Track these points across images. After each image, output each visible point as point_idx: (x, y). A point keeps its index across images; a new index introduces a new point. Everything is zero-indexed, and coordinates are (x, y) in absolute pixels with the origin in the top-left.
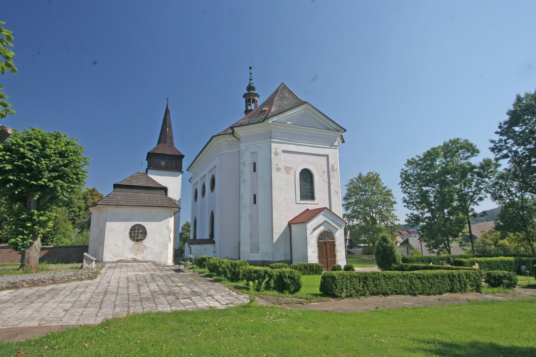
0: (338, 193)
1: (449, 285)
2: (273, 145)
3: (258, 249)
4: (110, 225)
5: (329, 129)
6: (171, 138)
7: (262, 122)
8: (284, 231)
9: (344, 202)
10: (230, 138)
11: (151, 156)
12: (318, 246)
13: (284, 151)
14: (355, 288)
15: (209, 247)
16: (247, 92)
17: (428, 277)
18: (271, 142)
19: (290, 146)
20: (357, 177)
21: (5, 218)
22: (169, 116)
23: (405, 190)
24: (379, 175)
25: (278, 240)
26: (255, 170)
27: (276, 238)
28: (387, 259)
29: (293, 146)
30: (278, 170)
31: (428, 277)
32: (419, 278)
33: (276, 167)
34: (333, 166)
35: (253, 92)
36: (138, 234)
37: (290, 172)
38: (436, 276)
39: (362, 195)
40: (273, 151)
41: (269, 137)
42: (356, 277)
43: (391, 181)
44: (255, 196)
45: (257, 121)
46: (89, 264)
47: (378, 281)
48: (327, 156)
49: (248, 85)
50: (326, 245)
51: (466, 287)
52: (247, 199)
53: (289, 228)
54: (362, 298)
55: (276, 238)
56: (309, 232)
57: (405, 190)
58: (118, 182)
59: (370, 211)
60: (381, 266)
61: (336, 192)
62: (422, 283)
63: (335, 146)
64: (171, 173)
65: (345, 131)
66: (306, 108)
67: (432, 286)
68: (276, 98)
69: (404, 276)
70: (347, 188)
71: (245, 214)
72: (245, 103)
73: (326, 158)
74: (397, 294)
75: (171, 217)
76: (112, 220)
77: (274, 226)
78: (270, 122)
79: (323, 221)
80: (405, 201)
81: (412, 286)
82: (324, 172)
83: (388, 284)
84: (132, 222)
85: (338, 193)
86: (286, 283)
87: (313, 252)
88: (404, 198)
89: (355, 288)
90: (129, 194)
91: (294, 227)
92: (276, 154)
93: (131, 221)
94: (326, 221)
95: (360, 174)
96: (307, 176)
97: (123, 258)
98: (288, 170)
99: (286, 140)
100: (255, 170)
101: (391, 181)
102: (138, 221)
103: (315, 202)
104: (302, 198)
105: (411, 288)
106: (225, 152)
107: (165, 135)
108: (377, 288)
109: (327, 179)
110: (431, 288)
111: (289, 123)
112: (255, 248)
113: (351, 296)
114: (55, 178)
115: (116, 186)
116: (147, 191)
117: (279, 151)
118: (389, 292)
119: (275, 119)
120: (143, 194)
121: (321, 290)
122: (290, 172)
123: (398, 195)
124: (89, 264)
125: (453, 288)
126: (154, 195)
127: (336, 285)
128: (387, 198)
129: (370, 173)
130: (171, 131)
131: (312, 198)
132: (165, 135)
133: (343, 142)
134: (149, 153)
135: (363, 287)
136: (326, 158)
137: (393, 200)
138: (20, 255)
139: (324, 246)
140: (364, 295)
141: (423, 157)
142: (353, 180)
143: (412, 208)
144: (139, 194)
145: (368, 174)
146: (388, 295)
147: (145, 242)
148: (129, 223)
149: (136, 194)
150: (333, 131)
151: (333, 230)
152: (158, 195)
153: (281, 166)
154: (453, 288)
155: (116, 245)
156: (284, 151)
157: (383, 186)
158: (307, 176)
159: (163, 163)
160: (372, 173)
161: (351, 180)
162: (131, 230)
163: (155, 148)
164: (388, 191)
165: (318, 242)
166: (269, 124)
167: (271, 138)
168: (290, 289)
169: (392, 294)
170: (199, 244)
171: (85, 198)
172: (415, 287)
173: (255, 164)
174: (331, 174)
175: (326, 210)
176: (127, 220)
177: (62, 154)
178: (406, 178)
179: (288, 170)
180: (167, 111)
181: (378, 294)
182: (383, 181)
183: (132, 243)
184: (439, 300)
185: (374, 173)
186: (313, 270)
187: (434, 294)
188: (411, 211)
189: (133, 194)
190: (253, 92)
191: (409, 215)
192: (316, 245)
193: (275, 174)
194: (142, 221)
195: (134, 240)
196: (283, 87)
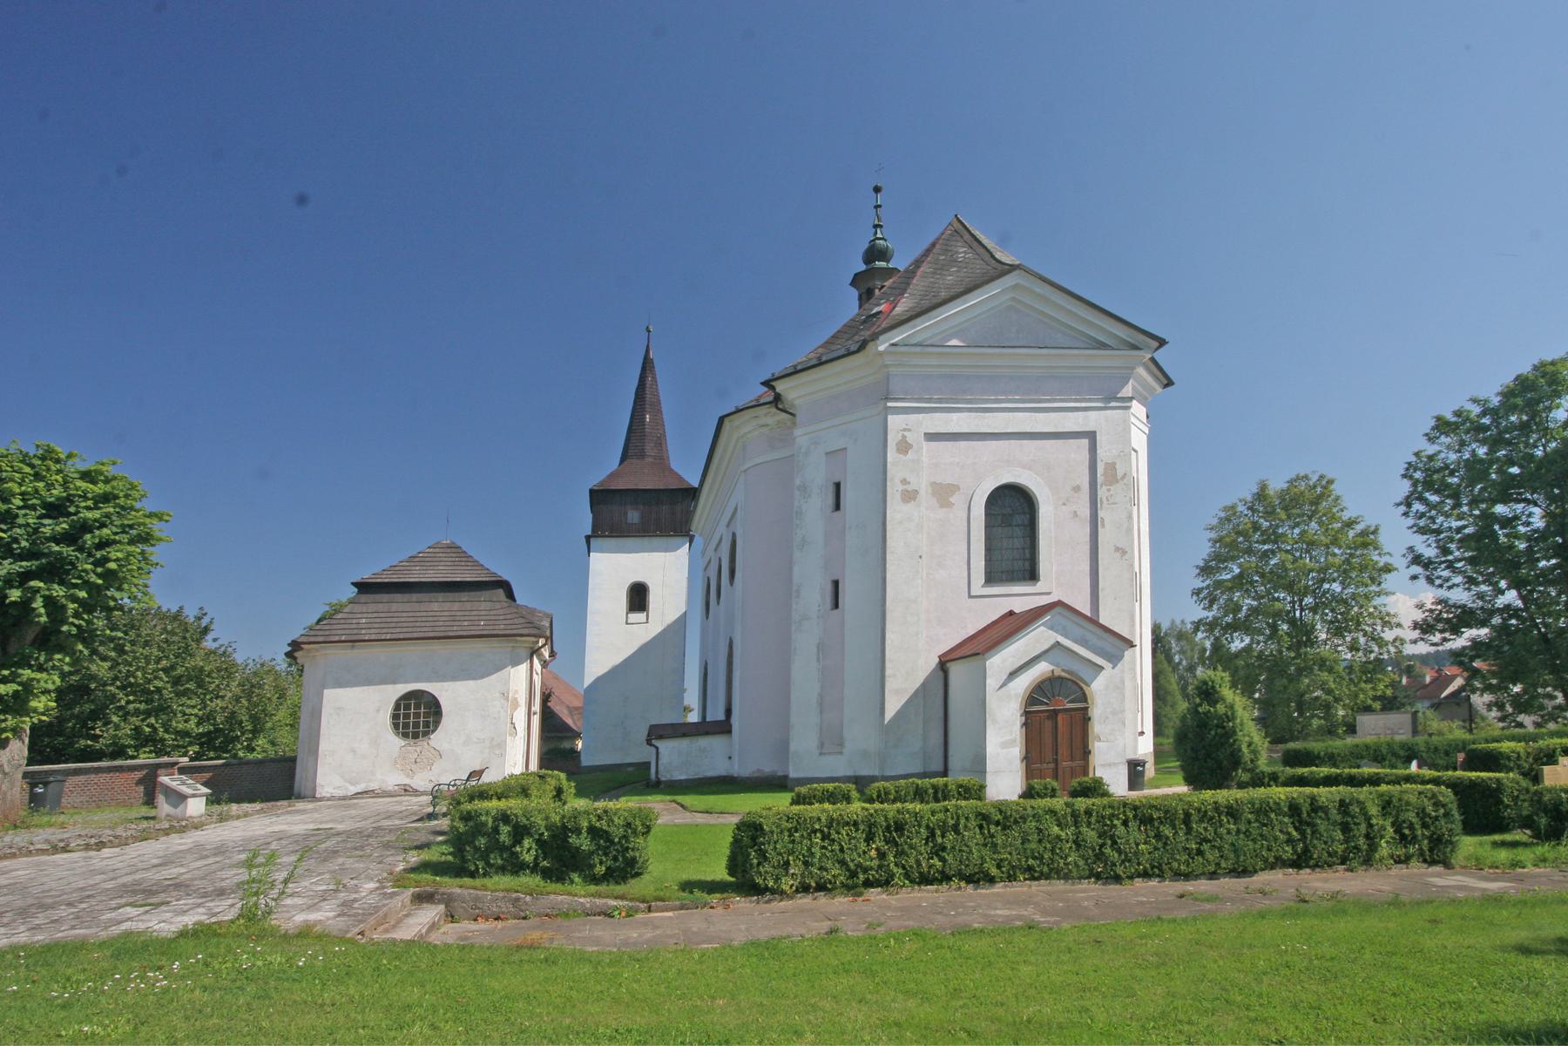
0: (1124, 552)
1: (1290, 841)
2: (895, 421)
3: (841, 745)
4: (333, 698)
5: (1104, 346)
6: (660, 442)
7: (858, 351)
8: (924, 685)
9: (1199, 583)
10: (771, 417)
11: (600, 497)
12: (1025, 724)
13: (932, 437)
14: (843, 863)
15: (715, 743)
16: (863, 267)
17: (1187, 815)
18: (888, 411)
19: (955, 416)
20: (1249, 498)
21: (114, 696)
22: (654, 378)
23: (1422, 523)
24: (1330, 482)
25: (900, 714)
26: (837, 507)
27: (892, 707)
28: (1208, 755)
30: (910, 496)
31: (1187, 815)
32: (1146, 821)
33: (901, 487)
34: (1111, 467)
35: (883, 264)
36: (417, 716)
38: (1233, 812)
39: (1265, 555)
41: (882, 395)
42: (855, 824)
43: (1374, 498)
44: (836, 584)
45: (843, 352)
46: (176, 807)
47: (951, 836)
48: (1091, 436)
49: (867, 245)
50: (1057, 721)
51: (1373, 847)
52: (813, 595)
53: (941, 674)
54: (874, 894)
55: (892, 707)
56: (992, 683)
57: (1422, 523)
58: (365, 575)
59: (1293, 602)
60: (1195, 780)
61: (1117, 549)
62: (1158, 836)
63: (1123, 399)
64: (656, 541)
65: (1162, 342)
66: (1016, 287)
67: (1205, 847)
68: (924, 268)
69: (1075, 815)
70: (1213, 535)
71: (805, 642)
72: (857, 303)
73: (1085, 442)
74: (1033, 878)
75: (516, 663)
76: (340, 684)
77: (888, 672)
78: (881, 348)
79: (1046, 647)
80: (1417, 560)
81: (1108, 850)
82: (1077, 489)
83: (995, 845)
85: (1124, 552)
86: (577, 849)
87: (1005, 745)
88: (1411, 549)
89: (843, 863)
90: (394, 607)
91: (956, 670)
92: (904, 447)
93: (394, 682)
95: (1263, 487)
96: (1012, 511)
97: (373, 786)
98: (943, 493)
99: (940, 401)
100: (837, 507)
101: (1374, 498)
102: (417, 680)
103: (1040, 586)
104: (990, 579)
105: (1100, 856)
106: (758, 461)
107: (640, 437)
108: (943, 860)
109: (1085, 512)
110: (1200, 852)
111: (954, 342)
112: (832, 740)
113: (821, 887)
114: (26, 576)
115: (364, 587)
116: (451, 596)
117: (914, 438)
118: (994, 871)
119: (898, 336)
120: (439, 608)
121: (732, 868)
123: (1398, 538)
124: (176, 807)
125: (1306, 850)
126: (468, 606)
127: (763, 855)
128: (1360, 558)
129: (1298, 478)
130: (659, 421)
131: (1032, 575)
132: (640, 437)
133: (1169, 383)
134: (591, 491)
135: (882, 855)
136: (1085, 442)
137: (1382, 561)
138: (142, 788)
139: (1048, 725)
140: (886, 883)
141: (1495, 401)
142: (1233, 507)
143: (1447, 580)
144: (423, 607)
145: (1290, 482)
146: (991, 880)
147: (438, 738)
148: (390, 687)
149: (416, 606)
150: (1115, 344)
151: (1084, 673)
152: (485, 607)
153: (922, 483)
154: (1306, 850)
155: (354, 751)
156: (932, 437)
157: (1346, 516)
158: (1012, 511)
159: (633, 516)
160: (1306, 477)
161: (1225, 509)
162: (397, 706)
163: (612, 476)
164: (1364, 533)
165: (1026, 713)
166: (881, 354)
167: (887, 399)
168: (592, 867)
169: (1011, 878)
170: (684, 735)
172: (1119, 852)
173: (838, 486)
174: (1102, 492)
175: (1058, 609)
176: (384, 681)
177: (55, 510)
178: (1427, 480)
179: (943, 493)
180: (647, 365)
181: (945, 878)
182: (1345, 502)
183: (399, 742)
184: (1182, 896)
185: (1314, 478)
187: (1213, 876)
188: (1443, 593)
189: (407, 607)
190: (883, 264)
191: (1429, 606)
192: (1018, 720)
193: (896, 511)
194: (429, 680)
195: (405, 735)
196: (960, 230)
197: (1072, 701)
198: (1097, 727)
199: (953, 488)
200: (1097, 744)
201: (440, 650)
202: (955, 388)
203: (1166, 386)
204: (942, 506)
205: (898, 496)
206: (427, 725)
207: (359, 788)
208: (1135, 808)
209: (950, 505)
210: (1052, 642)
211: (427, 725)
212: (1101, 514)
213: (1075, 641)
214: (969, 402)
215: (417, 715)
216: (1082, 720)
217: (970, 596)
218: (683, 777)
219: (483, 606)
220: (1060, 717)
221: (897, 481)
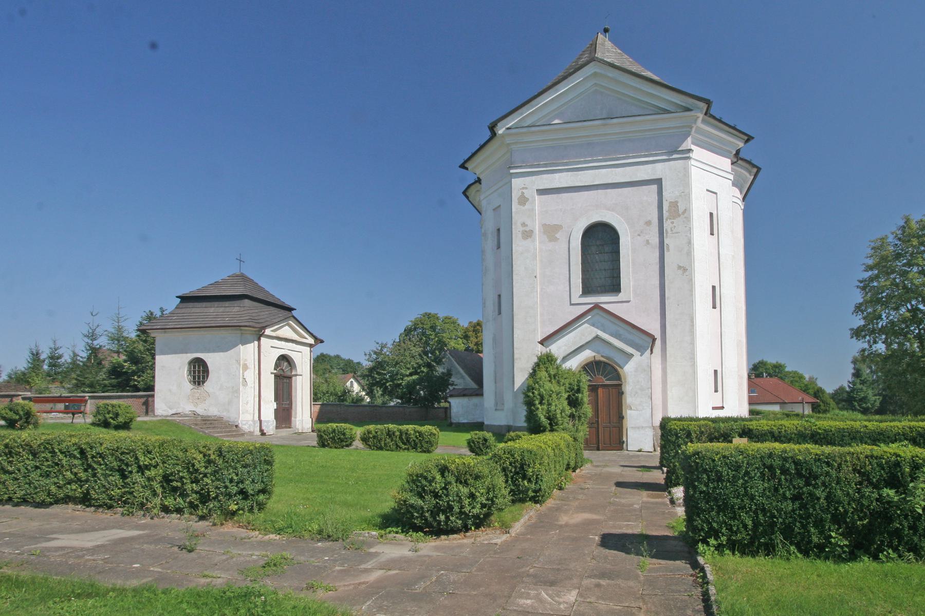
2: (516, 183)
5: (669, 112)
13: (541, 192)
19: (557, 175)
29: (565, 174)
30: (528, 235)
33: (521, 229)
34: (674, 205)
37: (557, 236)
40: (515, 195)
48: (658, 182)
58: (185, 291)
61: (679, 267)
63: (683, 152)
66: (595, 74)
77: (516, 356)
79: (589, 338)
82: (648, 223)
84: (189, 355)
85: (685, 270)
94: (597, 337)
96: (601, 242)
97: (180, 411)
98: (551, 231)
99: (546, 165)
102: (197, 352)
103: (621, 296)
111: (556, 121)
117: (531, 193)
122: (557, 236)
144: (206, 310)
148: (184, 355)
151: (618, 358)
156: (541, 192)
158: (601, 242)
167: (510, 168)
171: (466, 337)
174: (667, 225)
183: (192, 387)
186: (410, 443)
193: (519, 245)
197: (608, 380)
198: (630, 398)
199: (558, 228)
200: (629, 412)
201: (208, 335)
202: (557, 155)
203: (747, 141)
204: (550, 241)
205: (520, 235)
206: (203, 378)
207: (173, 412)
208: (797, 463)
209: (556, 239)
210: (594, 335)
211: (203, 378)
212: (666, 241)
213: (611, 335)
214: (566, 164)
215: (199, 372)
216: (617, 391)
217: (571, 304)
218: (465, 421)
219: (236, 309)
220: (600, 391)
221: (519, 224)
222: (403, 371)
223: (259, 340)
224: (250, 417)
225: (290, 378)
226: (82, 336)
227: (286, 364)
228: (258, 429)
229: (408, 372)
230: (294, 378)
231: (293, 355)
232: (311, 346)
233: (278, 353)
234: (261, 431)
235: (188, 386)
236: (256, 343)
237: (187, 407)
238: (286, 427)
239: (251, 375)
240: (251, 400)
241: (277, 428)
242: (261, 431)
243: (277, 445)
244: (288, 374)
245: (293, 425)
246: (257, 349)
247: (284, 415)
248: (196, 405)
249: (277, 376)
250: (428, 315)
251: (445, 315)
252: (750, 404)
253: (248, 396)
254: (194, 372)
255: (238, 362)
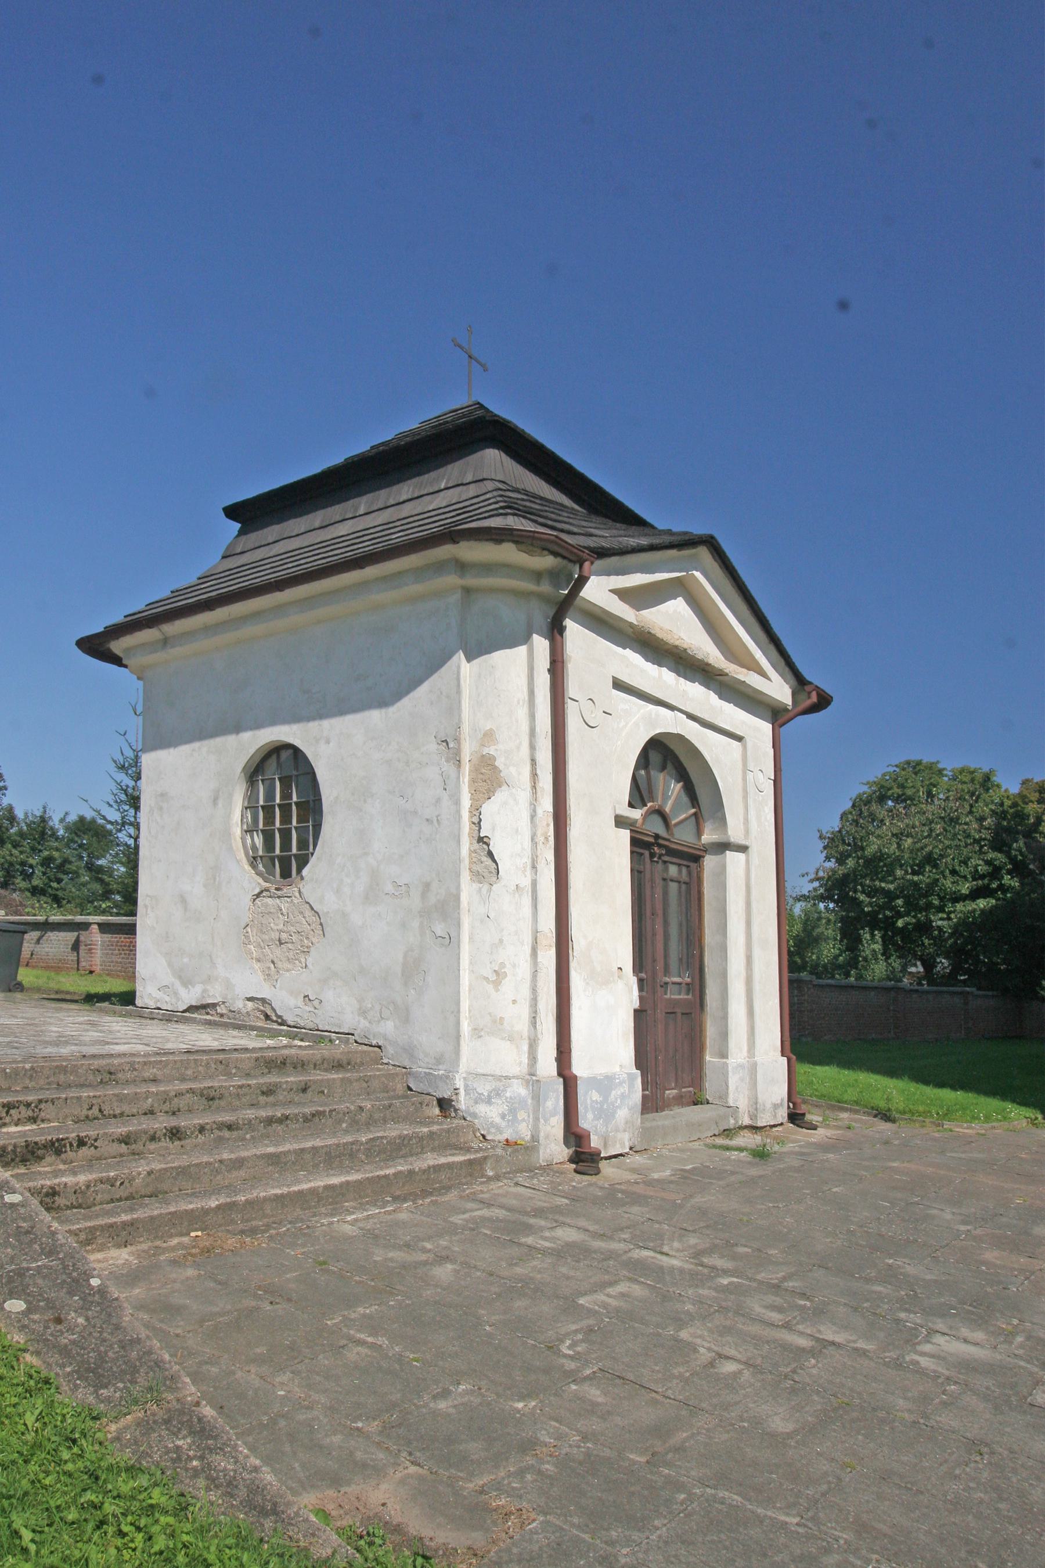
84: (246, 736)
102: (275, 720)
148: (231, 740)
206: (303, 844)
222: (948, 883)
223: (555, 630)
224: (509, 1059)
225: (693, 858)
226: (112, 768)
227: (676, 788)
228: (555, 1126)
229: (965, 888)
230: (709, 862)
231: (712, 748)
232: (776, 715)
233: (641, 724)
234: (574, 1136)
235: (245, 879)
236: (541, 644)
237: (240, 982)
238: (680, 1101)
239: (514, 821)
240: (516, 957)
241: (651, 1104)
242: (574, 1136)
243: (453, 708)
244: (683, 836)
245: (710, 1088)
246: (543, 680)
247: (673, 1038)
248: (272, 972)
249: (642, 846)
250: (916, 767)
251: (958, 765)
252: (134, 925)
253: (501, 932)
254: (268, 810)
255: (450, 745)
